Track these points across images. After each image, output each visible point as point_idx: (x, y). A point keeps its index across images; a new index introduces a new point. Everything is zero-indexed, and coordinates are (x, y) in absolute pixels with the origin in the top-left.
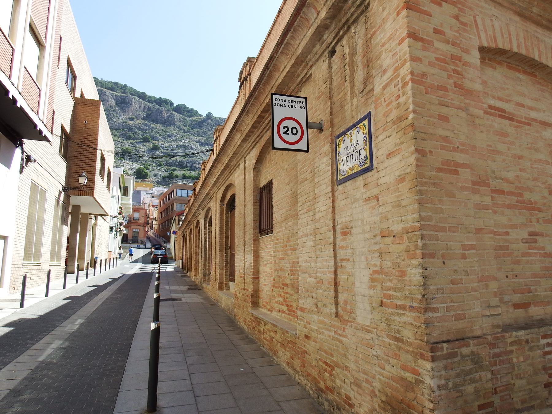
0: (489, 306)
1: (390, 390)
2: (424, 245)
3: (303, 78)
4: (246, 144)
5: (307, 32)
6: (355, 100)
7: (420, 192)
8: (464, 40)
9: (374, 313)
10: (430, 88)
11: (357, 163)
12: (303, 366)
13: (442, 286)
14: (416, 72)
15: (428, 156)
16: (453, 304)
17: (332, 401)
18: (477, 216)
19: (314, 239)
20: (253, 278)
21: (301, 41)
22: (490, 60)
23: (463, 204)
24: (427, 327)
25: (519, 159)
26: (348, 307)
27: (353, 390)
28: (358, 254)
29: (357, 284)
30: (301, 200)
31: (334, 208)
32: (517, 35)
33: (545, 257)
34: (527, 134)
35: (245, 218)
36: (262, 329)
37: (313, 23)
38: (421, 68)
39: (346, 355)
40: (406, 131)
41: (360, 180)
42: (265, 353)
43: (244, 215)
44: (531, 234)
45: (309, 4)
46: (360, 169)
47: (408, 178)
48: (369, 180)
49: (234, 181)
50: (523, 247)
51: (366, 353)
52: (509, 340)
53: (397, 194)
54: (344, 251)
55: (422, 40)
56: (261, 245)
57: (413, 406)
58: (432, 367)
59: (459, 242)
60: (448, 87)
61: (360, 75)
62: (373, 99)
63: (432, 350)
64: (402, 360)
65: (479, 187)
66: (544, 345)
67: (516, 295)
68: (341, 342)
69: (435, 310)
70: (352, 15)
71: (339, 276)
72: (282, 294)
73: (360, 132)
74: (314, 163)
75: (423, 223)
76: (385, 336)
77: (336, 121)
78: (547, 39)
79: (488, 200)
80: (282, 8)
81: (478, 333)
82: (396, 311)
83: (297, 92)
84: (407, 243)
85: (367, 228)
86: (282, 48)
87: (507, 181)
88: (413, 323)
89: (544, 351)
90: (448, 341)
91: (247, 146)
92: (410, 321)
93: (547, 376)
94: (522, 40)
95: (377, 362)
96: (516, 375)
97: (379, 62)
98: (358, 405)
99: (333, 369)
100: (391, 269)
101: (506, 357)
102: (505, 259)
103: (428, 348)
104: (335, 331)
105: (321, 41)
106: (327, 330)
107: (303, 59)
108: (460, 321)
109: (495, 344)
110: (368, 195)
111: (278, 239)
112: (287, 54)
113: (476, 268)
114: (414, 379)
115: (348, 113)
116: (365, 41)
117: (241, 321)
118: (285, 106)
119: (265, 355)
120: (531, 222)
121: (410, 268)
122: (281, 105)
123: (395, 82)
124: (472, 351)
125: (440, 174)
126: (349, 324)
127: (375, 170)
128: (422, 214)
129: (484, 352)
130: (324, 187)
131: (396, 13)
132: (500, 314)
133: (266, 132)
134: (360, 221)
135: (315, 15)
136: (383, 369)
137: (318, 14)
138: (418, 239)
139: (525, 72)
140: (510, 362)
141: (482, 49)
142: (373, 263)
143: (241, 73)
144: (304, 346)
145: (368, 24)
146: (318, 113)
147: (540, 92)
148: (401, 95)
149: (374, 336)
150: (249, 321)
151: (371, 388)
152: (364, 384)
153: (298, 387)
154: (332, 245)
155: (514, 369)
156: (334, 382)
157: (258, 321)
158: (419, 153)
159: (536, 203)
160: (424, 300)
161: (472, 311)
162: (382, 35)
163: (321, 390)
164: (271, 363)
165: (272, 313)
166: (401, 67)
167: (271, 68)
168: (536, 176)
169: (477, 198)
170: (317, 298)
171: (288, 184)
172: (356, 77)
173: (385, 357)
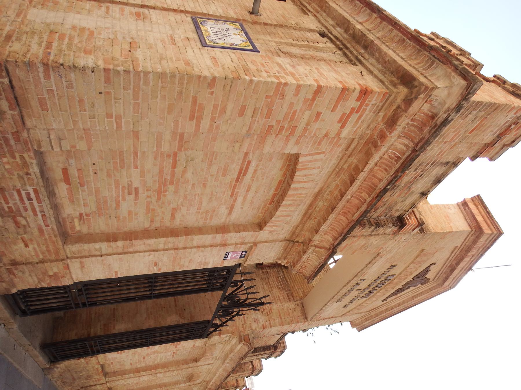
0: (60, 139)
2: (119, 72)
5: (347, 13)
6: (274, 44)
7: (173, 76)
9: (43, 25)
10: (271, 101)
13: (75, 88)
14: (286, 88)
15: (209, 90)
16: (56, 98)
18: (150, 135)
22: (288, 166)
23: (161, 121)
24: (25, 63)
25: (203, 184)
28: (114, 22)
29: (78, 16)
31: (167, 10)
32: (304, 189)
33: (116, 200)
34: (224, 192)
37: (354, 18)
44: (136, 189)
45: (372, 15)
47: (189, 69)
48: (193, 43)
50: (124, 181)
52: (26, 156)
53: (174, 59)
55: (314, 99)
59: (124, 112)
61: (295, 51)
65: (178, 140)
66: (27, 190)
67: (76, 171)
69: (47, 76)
70: (351, 52)
73: (242, 42)
75: (142, 74)
77: (258, 27)
78: (297, 213)
79: (166, 148)
81: (29, 123)
84: (121, 59)
85: (142, 33)
87: (184, 172)
89: (21, 190)
92: (32, 50)
94: (299, 192)
101: (6, 150)
102: (112, 163)
105: (336, 26)
107: (324, 8)
108: (38, 105)
109: (20, 141)
113: (98, 128)
115: (262, 37)
116: (325, 59)
120: (147, 190)
121: (94, 58)
124: (5, 112)
125: (191, 101)
128: (151, 74)
132: (53, 149)
134: (150, 29)
135: (360, 21)
137: (360, 23)
138: (124, 67)
139: (274, 195)
141: (297, 156)
146: (269, 13)
147: (257, 206)
158: (211, 80)
159: (165, 196)
161: (52, 118)
168: (189, 197)
169: (167, 136)
172: (295, 48)
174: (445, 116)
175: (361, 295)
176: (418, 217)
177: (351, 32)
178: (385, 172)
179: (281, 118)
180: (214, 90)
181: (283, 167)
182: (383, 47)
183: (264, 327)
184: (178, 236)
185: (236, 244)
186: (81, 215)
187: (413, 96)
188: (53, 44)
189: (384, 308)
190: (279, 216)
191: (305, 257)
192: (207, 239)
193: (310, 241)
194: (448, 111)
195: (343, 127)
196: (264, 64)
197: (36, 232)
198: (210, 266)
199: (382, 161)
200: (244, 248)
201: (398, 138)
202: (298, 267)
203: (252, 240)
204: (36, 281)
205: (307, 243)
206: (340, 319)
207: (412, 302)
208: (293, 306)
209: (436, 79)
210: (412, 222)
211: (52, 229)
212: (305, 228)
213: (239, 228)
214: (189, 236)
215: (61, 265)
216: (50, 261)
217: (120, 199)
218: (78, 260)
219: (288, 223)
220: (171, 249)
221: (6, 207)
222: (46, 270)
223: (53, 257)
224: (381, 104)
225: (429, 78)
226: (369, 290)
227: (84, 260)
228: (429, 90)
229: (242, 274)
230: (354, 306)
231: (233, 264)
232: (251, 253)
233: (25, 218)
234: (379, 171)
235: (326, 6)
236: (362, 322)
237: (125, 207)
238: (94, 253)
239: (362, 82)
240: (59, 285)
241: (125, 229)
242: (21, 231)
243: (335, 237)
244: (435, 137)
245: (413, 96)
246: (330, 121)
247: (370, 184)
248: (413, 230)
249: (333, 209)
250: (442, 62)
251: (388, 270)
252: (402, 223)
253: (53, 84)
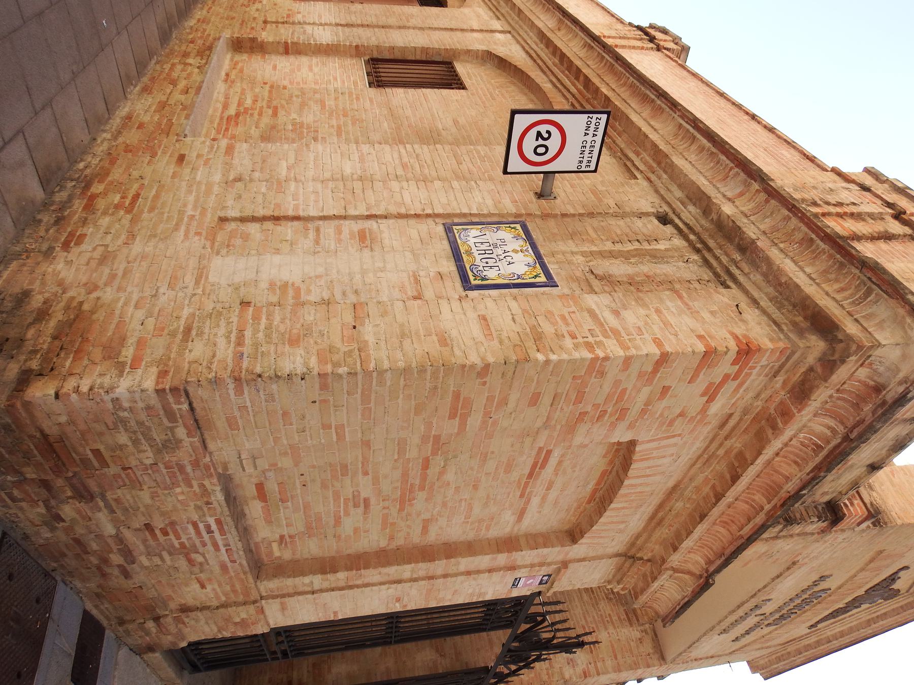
0: (254, 458)
1: (102, 318)
2: (340, 376)
3: (632, 162)
4: (535, 38)
6: (580, 259)
7: (422, 370)
8: (648, 422)
11: (478, 262)
12: (128, 149)
14: (607, 363)
16: (251, 414)
17: (70, 207)
19: (355, 177)
20: (286, 43)
21: (693, 165)
22: (617, 451)
23: (405, 425)
24: (210, 381)
26: (238, 242)
27: (94, 249)
29: (277, 259)
30: (424, 151)
31: (406, 216)
32: (647, 485)
34: (509, 494)
35: (400, 27)
36: (190, 61)
37: (718, 189)
38: (613, 372)
39: (155, 236)
40: (518, 349)
41: (449, 267)
42: (145, 67)
43: (404, 27)
44: (366, 501)
45: (749, 185)
46: (468, 267)
48: (448, 283)
49: (470, 6)
50: (348, 491)
51: (161, 276)
52: (206, 483)
53: (422, 333)
54: (332, 234)
55: (655, 371)
56: (348, 62)
57: (80, 359)
58: (147, 390)
59: (348, 421)
60: (581, 405)
61: (619, 269)
62: (578, 292)
63: (174, 390)
64: (154, 340)
67: (276, 485)
68: (177, 228)
69: (239, 391)
70: (717, 258)
71: (290, 224)
72: (259, 104)
73: (526, 268)
74: (485, 180)
75: (375, 374)
76: (191, 310)
77: (552, 223)
78: (638, 516)
80: (759, 122)
81: (211, 446)
82: (234, 329)
83: (610, 148)
86: (688, 127)
87: (442, 473)
88: (216, 359)
90: (192, 409)
91: (531, 38)
93: (162, 526)
95: (146, 294)
96: (156, 492)
97: (633, 303)
98: (69, 259)
99: (129, 211)
100: (302, 321)
103: (176, 383)
104: (194, 216)
105: (686, 200)
106: (197, 201)
107: (663, 165)
110: (424, 280)
111: (358, 99)
112: (676, 135)
113: (310, 442)
114: (125, 359)
115: (561, 246)
116: (670, 279)
117: (204, 12)
118: (586, 134)
119: (141, 66)
122: (588, 128)
123: (597, 331)
126: (208, 244)
127: (464, 294)
128: (389, 372)
129: (184, 455)
130: (444, 200)
131: (703, 333)
132: (244, 470)
133: (551, 81)
135: (729, 194)
136: (136, 307)
137: (729, 199)
139: (595, 491)
140: (175, 484)
141: (632, 444)
142: (312, 288)
143: (665, 31)
144: (164, 153)
145: (697, 285)
148: (575, 341)
149: (190, 291)
150: (205, 30)
151: (101, 283)
152: (107, 271)
153: (86, 138)
154: (342, 213)
155: (165, 489)
156: (105, 213)
157: (206, 51)
158: (482, 369)
159: (412, 505)
160: (254, 377)
162: (673, 309)
163: (88, 186)
164: (126, 82)
165: (224, 82)
166: (617, 341)
167: (659, 102)
168: (450, 504)
169: (416, 440)
170: (251, 180)
171: (456, 122)
172: (617, 262)
173: (157, 309)
174: (901, 389)
175: (766, 622)
176: (867, 501)
177: (714, 216)
178: (794, 466)
179: (600, 400)
180: (487, 379)
181: (606, 454)
182: (774, 254)
183: (586, 675)
184: (435, 561)
185: (532, 566)
186: (282, 537)
187: (836, 356)
188: (246, 333)
189: (813, 639)
190: (605, 524)
191: (656, 585)
192: (483, 561)
193: (664, 561)
194: (906, 382)
195: (711, 400)
196: (567, 317)
197: (217, 570)
198: (489, 597)
199: (789, 449)
200: (545, 570)
201: (815, 416)
202: (643, 598)
203: (560, 558)
204: (215, 629)
205: (658, 565)
206: (728, 658)
207: (869, 631)
208: (638, 635)
209: (877, 324)
210: (855, 510)
211: (241, 564)
212: (653, 539)
213: (538, 540)
214: (452, 560)
215: (252, 609)
216: (237, 604)
217: (342, 514)
218: (278, 600)
219: (621, 531)
220: (423, 579)
221: (176, 543)
222: (230, 616)
223: (241, 598)
224: (777, 364)
225: (865, 325)
226: (781, 614)
227: (286, 599)
228: (865, 352)
229: (544, 604)
230: (754, 638)
231: (528, 593)
232: (559, 577)
233: (203, 555)
234: (782, 464)
235: (667, 163)
236: (771, 663)
237: (348, 525)
238: (301, 589)
239: (739, 331)
240: (249, 633)
241: (349, 551)
242: (196, 569)
243: (709, 559)
244: (886, 422)
245: (836, 356)
246: (689, 396)
247: (769, 482)
248: (859, 524)
249: (703, 517)
250: (886, 293)
251: (815, 584)
252: (836, 514)
253: (247, 400)
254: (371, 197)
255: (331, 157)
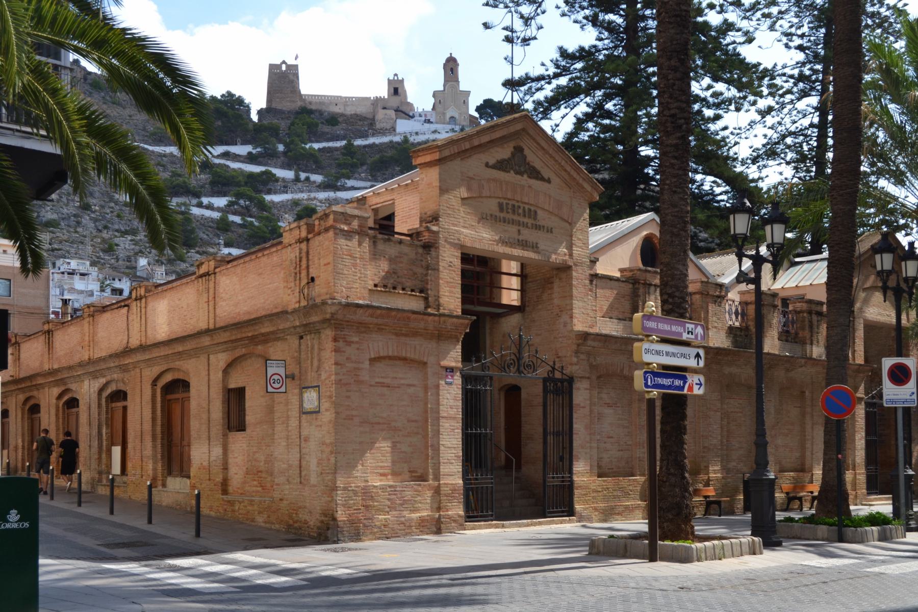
30: (277, 415)
56: (230, 440)
61: (316, 363)
157: (231, 503)
254: (294, 437)
255: (280, 450)
